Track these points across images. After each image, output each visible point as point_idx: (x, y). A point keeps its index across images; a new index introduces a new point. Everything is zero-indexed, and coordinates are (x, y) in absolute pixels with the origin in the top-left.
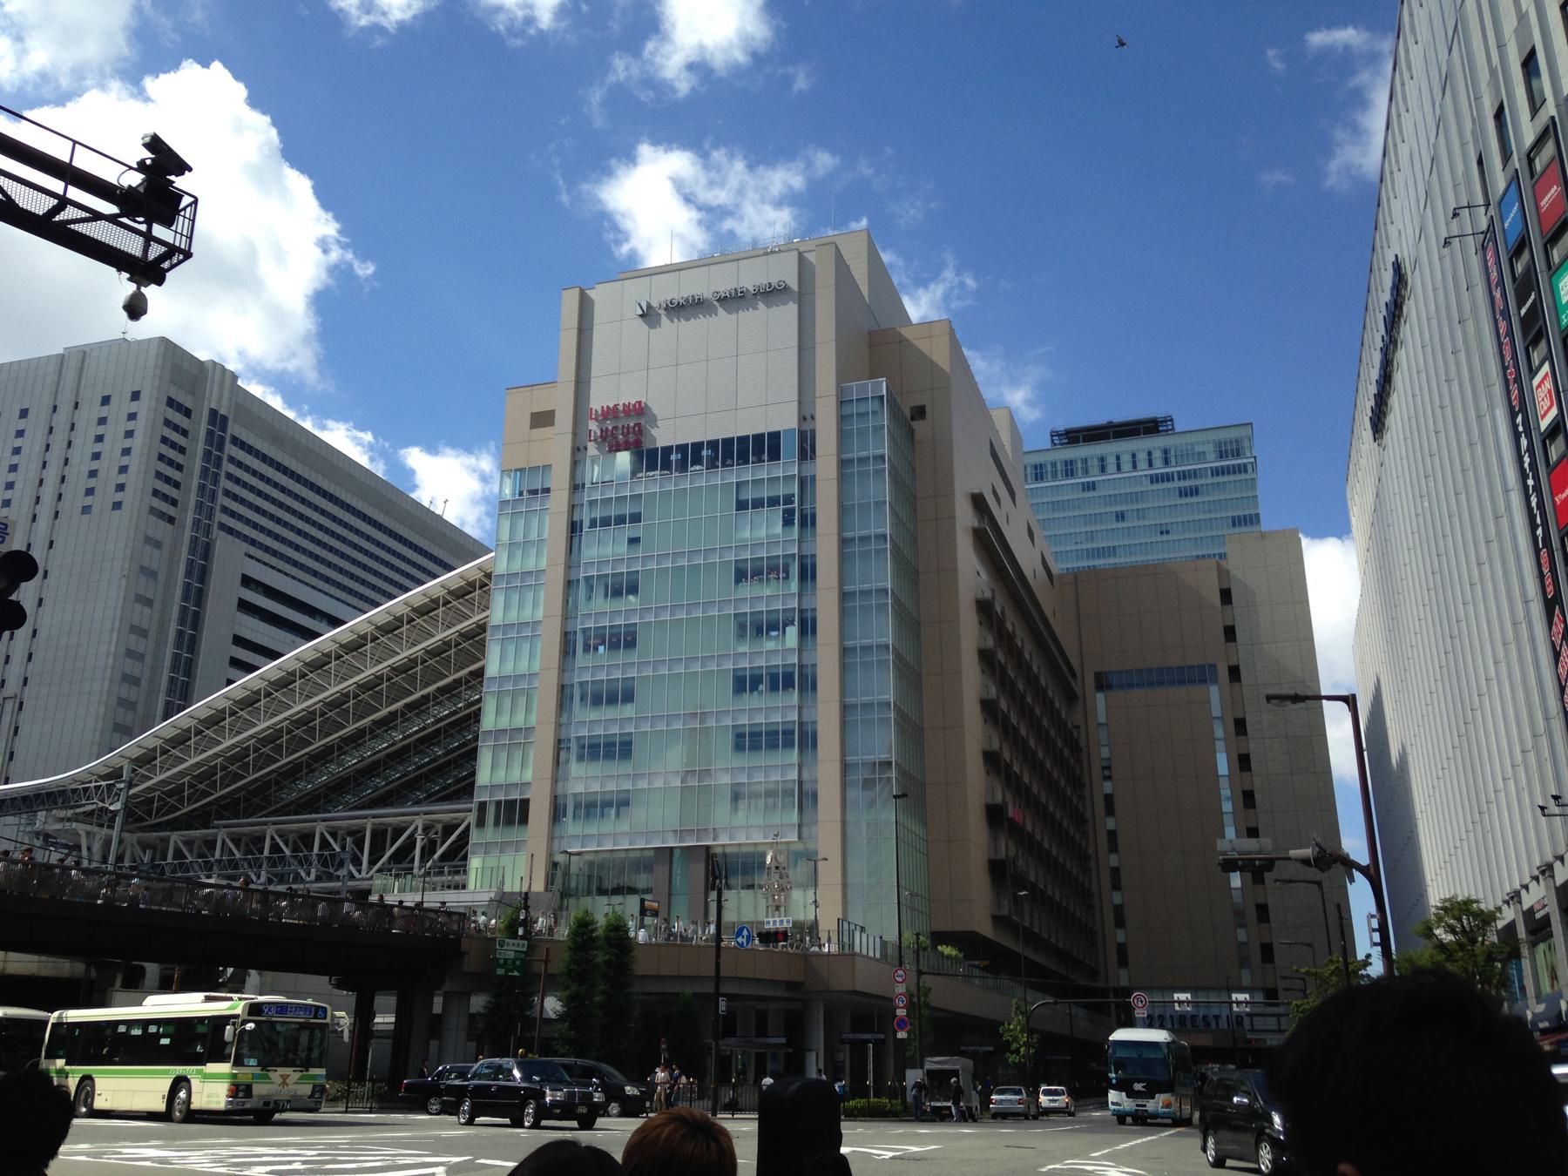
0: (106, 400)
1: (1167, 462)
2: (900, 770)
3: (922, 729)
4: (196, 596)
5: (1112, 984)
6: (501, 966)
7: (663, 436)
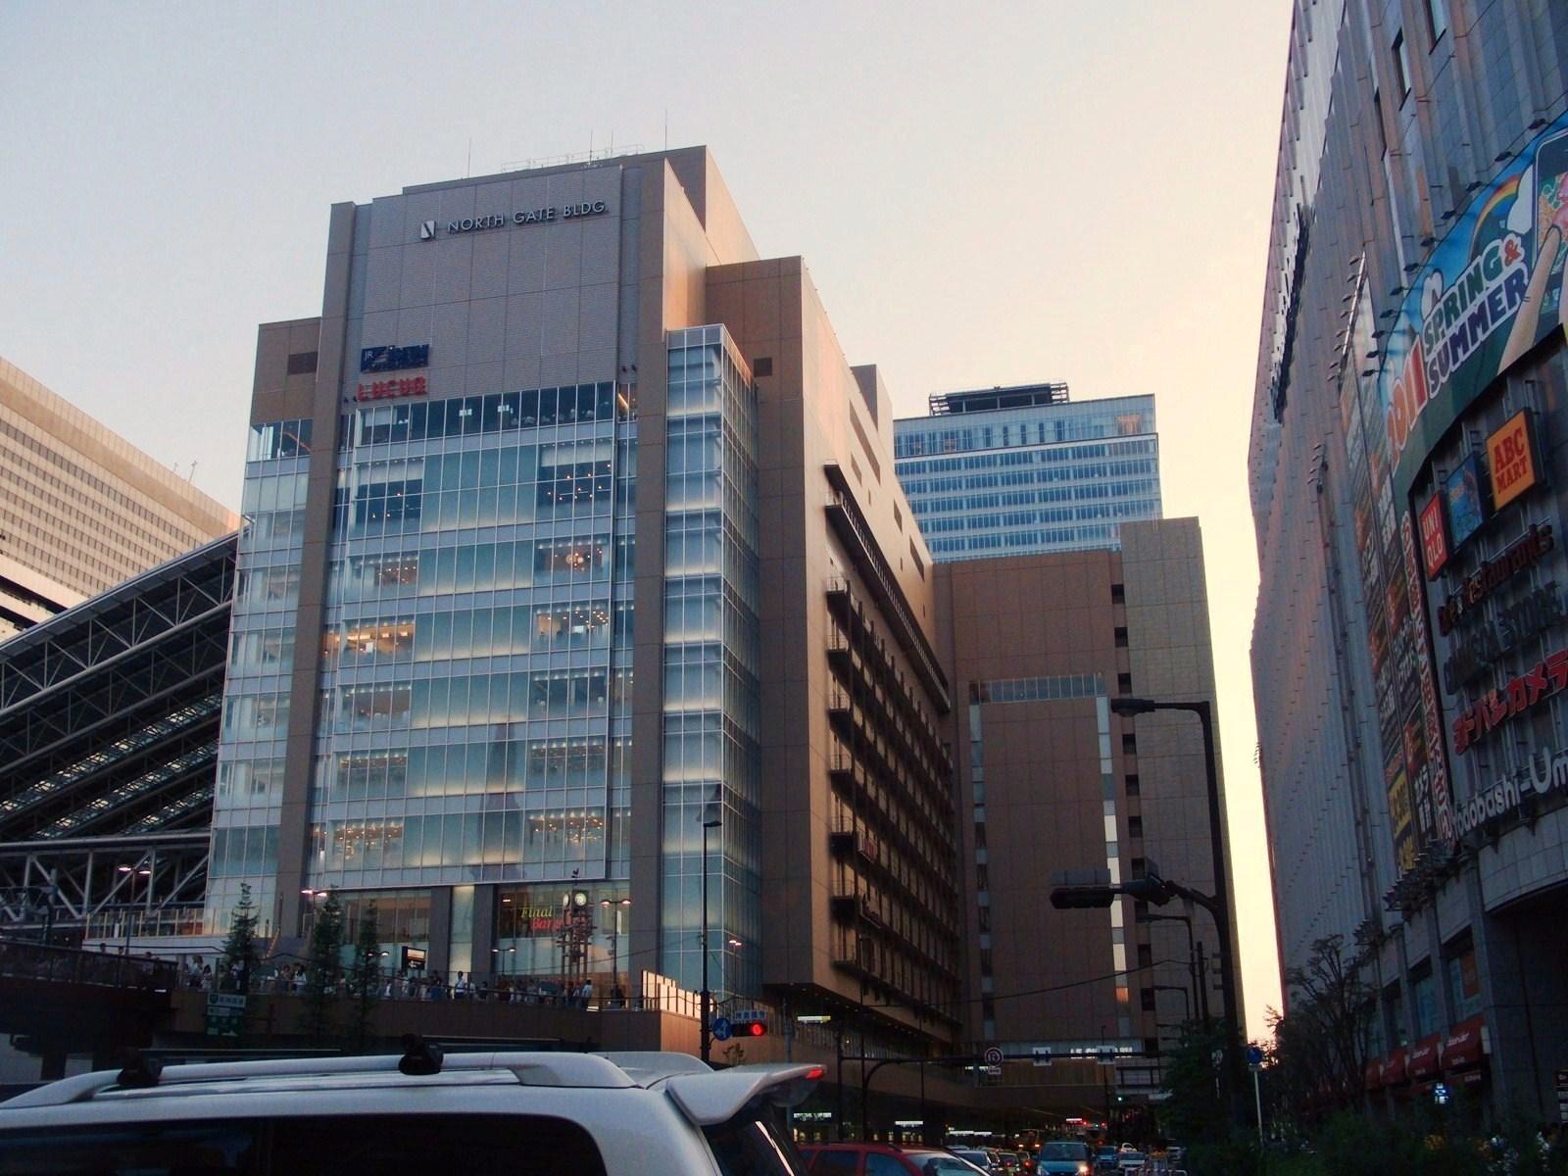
1: (1060, 439)
7: (442, 383)
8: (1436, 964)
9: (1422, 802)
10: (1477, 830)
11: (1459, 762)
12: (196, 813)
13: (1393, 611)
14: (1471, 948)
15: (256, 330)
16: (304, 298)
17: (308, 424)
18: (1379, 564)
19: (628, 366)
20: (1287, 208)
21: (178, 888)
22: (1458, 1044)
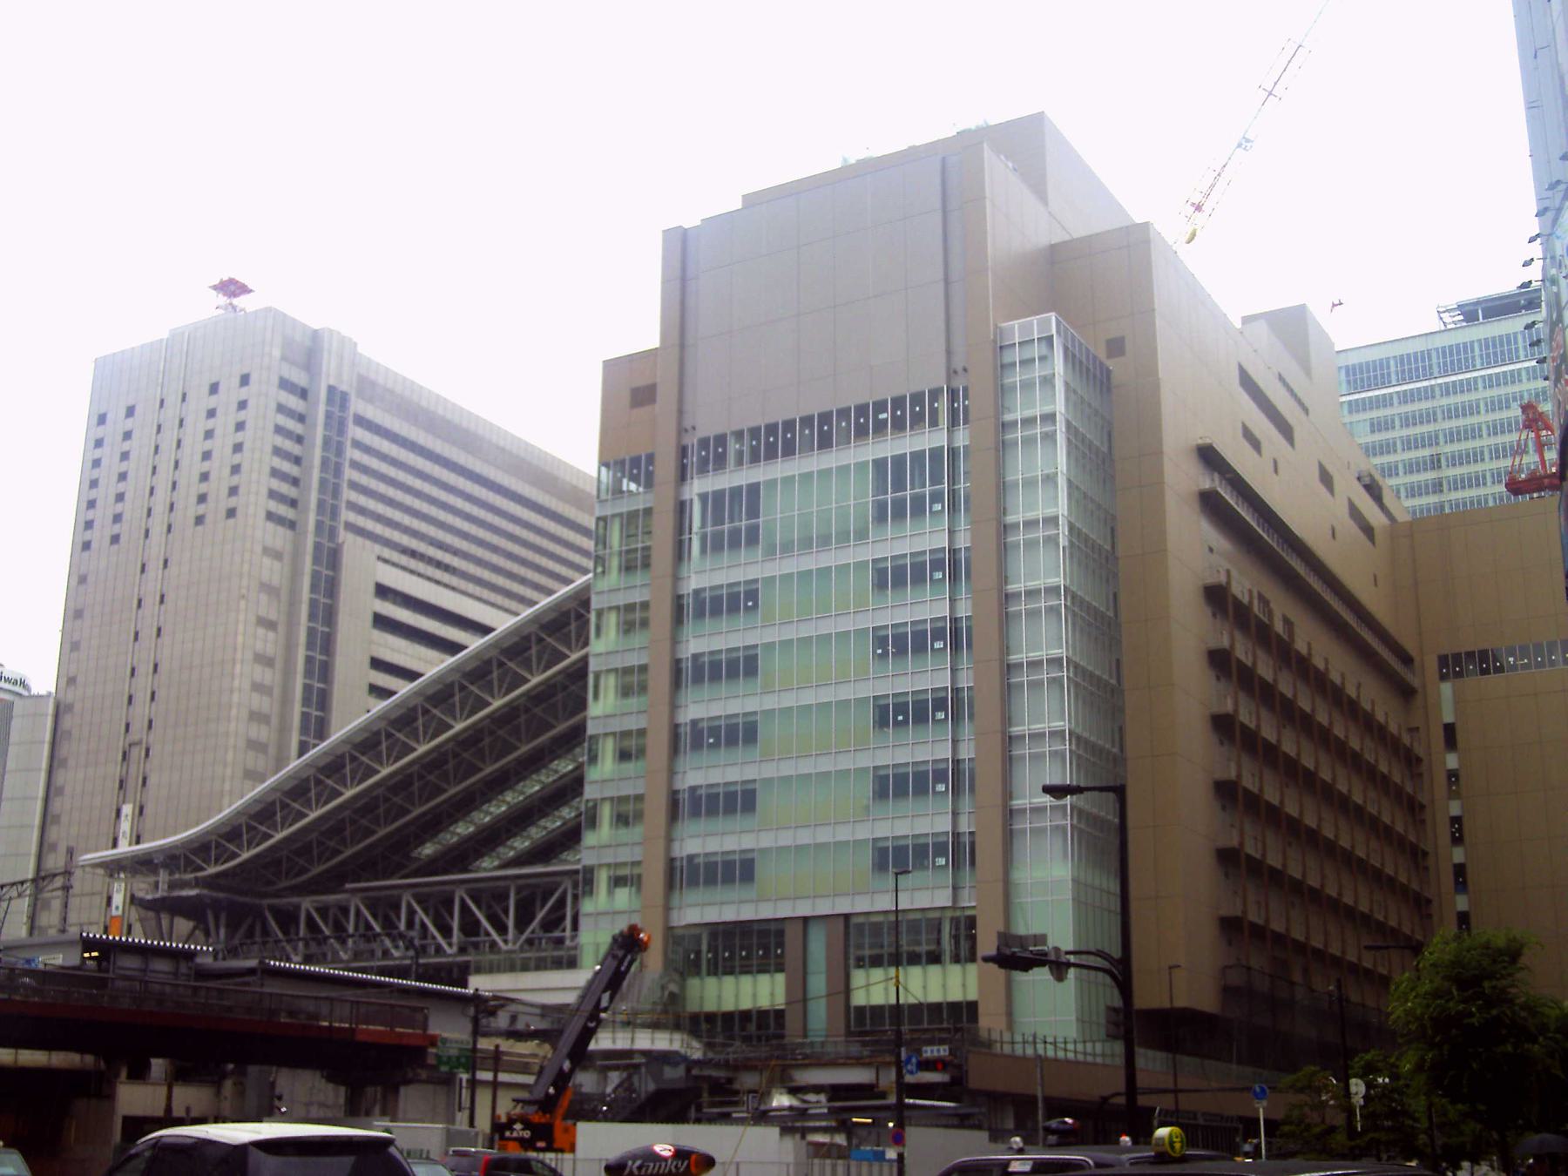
0: (115, 539)
4: (325, 614)
15: (601, 366)
17: (651, 459)
19: (960, 369)
21: (540, 916)
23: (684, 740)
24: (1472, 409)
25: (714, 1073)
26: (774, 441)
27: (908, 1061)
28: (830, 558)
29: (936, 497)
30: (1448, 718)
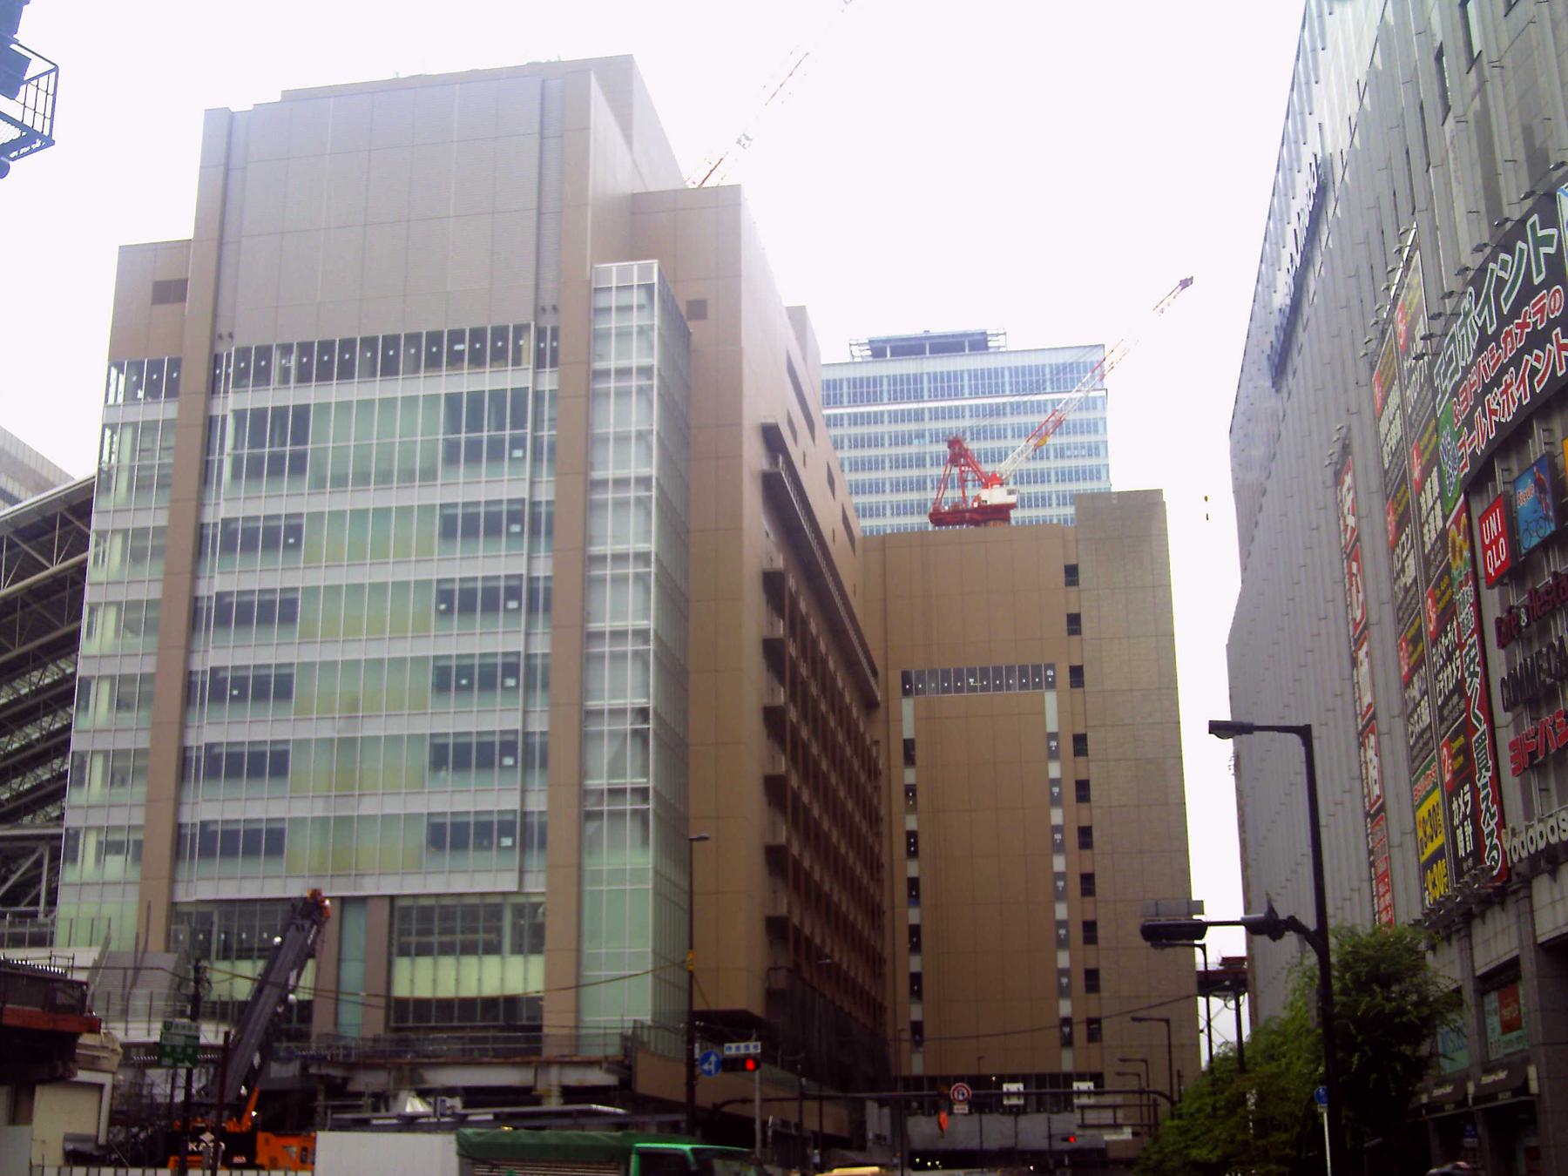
2: (661, 721)
3: (687, 819)
5: (905, 1073)
6: (168, 1055)
8: (1468, 995)
9: (1462, 823)
10: (1534, 859)
11: (1511, 784)
12: (12, 805)
13: (1433, 616)
14: (1518, 977)
16: (174, 218)
17: (176, 364)
18: (1417, 564)
19: (549, 308)
20: (1299, 159)
22: (1494, 1082)
23: (200, 691)
24: (876, 442)
25: (333, 1072)
26: (327, 360)
27: (706, 1058)
28: (394, 498)
29: (518, 443)
30: (908, 733)
